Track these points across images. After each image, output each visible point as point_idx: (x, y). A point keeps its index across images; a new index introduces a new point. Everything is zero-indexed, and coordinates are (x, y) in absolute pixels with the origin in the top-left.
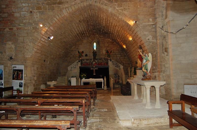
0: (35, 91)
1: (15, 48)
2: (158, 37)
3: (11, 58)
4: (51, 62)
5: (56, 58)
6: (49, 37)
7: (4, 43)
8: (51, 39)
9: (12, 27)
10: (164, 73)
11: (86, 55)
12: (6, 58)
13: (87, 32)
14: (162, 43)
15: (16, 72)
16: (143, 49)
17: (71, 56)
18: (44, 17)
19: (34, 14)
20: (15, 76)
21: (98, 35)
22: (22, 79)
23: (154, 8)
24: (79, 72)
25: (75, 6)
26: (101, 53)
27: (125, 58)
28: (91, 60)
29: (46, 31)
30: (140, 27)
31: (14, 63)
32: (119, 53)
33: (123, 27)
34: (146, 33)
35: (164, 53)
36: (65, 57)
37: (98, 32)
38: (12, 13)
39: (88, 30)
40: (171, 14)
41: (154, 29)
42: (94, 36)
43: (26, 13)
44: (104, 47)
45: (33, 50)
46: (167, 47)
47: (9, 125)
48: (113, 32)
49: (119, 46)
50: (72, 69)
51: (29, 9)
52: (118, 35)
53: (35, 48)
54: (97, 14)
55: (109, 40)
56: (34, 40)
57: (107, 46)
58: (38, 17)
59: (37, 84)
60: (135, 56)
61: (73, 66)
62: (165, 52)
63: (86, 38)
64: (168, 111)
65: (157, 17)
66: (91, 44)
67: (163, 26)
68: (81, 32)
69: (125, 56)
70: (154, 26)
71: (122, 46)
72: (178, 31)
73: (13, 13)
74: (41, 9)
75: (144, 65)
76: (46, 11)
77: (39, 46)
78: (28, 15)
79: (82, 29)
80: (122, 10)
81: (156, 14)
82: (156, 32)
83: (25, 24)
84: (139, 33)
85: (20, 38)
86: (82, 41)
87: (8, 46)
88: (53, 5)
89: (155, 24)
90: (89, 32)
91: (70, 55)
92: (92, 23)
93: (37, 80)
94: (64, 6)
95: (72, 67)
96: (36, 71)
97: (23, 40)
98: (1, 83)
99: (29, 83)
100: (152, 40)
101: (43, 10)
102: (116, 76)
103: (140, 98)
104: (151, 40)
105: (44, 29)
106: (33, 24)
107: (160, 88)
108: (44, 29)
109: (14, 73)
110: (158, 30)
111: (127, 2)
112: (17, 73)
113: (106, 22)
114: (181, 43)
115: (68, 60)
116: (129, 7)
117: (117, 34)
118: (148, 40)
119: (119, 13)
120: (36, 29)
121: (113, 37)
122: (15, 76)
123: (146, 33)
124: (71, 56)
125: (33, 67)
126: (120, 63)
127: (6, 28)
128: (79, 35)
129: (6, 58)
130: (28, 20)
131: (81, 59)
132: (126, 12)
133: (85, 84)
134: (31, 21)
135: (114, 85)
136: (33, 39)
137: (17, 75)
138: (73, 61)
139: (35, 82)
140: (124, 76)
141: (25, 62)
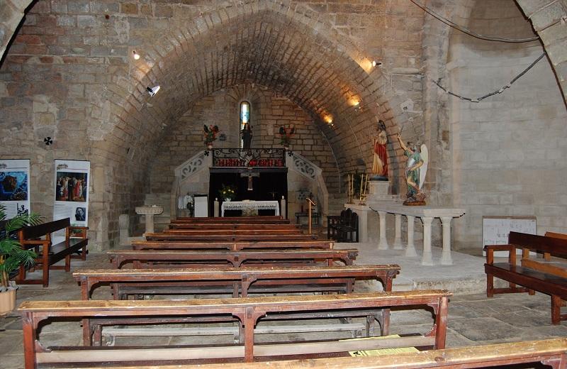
1: (60, 114)
2: (429, 104)
3: (48, 141)
6: (148, 88)
7: (25, 97)
9: (50, 54)
10: (438, 190)
11: (223, 137)
12: (31, 140)
14: (438, 119)
15: (68, 179)
16: (387, 130)
17: (180, 138)
18: (143, 34)
19: (114, 24)
20: (64, 190)
21: (255, 85)
22: (83, 199)
23: (421, 33)
25: (230, 11)
26: (263, 133)
27: (326, 149)
29: (147, 71)
30: (388, 78)
31: (58, 153)
33: (340, 72)
34: (401, 93)
35: (440, 144)
37: (259, 77)
38: (51, 16)
40: (461, 52)
41: (419, 83)
43: (91, 19)
44: (271, 117)
46: (449, 128)
47: (159, 302)
48: (303, 81)
49: (310, 117)
50: (185, 173)
51: (102, 10)
52: (317, 89)
54: (275, 34)
55: (285, 98)
58: (125, 33)
60: (359, 144)
62: (442, 142)
63: (222, 90)
64: (485, 265)
65: (428, 57)
67: (440, 79)
69: (325, 143)
70: (419, 76)
71: (319, 118)
72: (484, 98)
73: (55, 17)
74: (136, 12)
75: (410, 172)
76: (149, 19)
78: (97, 24)
80: (346, 31)
81: (426, 48)
82: (423, 91)
83: (88, 48)
84: (383, 91)
85: (75, 86)
87: (36, 107)
88: (169, 5)
89: (423, 73)
92: (252, 53)
94: (199, 10)
95: (186, 169)
97: (82, 93)
98: (23, 209)
99: (100, 210)
100: (412, 111)
101: (140, 13)
103: (393, 246)
104: (410, 110)
105: (142, 67)
106: (112, 51)
107: (452, 222)
108: (142, 67)
109: (62, 183)
110: (430, 86)
111: (360, 12)
112: (70, 182)
113: (295, 55)
114: (480, 122)
115: (171, 149)
116: (363, 25)
117: (317, 86)
118: (403, 111)
119: (338, 38)
120: (121, 65)
121: (300, 92)
122: (62, 189)
123: (401, 93)
124: (180, 138)
127: (31, 57)
129: (31, 140)
130: (96, 40)
131: (210, 147)
132: (354, 38)
133: (231, 213)
134: (105, 42)
135: (298, 217)
137: (71, 186)
140: (326, 195)
141: (90, 154)
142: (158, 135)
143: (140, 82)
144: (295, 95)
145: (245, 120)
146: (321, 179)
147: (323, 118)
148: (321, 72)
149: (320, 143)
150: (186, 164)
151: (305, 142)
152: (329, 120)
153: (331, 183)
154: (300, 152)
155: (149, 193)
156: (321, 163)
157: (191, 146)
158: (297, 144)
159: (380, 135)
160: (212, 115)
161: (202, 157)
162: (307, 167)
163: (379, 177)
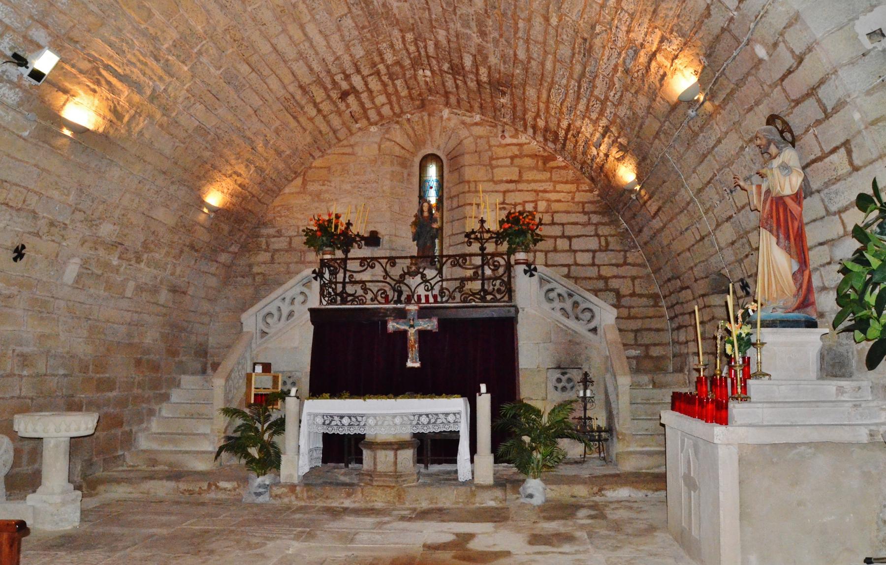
13: (374, 84)
27: (629, 260)
28: (394, 265)
32: (589, 223)
39: (381, 67)
42: (425, 114)
44: (490, 186)
55: (523, 139)
57: (511, 181)
61: (279, 309)
63: (373, 129)
79: (329, 47)
86: (348, 150)
90: (385, 78)
91: (269, 236)
95: (270, 314)
102: (564, 378)
115: (256, 269)
118: (867, 44)
126: (596, 292)
128: (319, 94)
138: (288, 264)
146: (614, 335)
149: (614, 243)
151: (577, 244)
152: (626, 174)
153: (647, 346)
156: (618, 295)
158: (555, 250)
160: (348, 187)
162: (576, 304)
163: (780, 314)
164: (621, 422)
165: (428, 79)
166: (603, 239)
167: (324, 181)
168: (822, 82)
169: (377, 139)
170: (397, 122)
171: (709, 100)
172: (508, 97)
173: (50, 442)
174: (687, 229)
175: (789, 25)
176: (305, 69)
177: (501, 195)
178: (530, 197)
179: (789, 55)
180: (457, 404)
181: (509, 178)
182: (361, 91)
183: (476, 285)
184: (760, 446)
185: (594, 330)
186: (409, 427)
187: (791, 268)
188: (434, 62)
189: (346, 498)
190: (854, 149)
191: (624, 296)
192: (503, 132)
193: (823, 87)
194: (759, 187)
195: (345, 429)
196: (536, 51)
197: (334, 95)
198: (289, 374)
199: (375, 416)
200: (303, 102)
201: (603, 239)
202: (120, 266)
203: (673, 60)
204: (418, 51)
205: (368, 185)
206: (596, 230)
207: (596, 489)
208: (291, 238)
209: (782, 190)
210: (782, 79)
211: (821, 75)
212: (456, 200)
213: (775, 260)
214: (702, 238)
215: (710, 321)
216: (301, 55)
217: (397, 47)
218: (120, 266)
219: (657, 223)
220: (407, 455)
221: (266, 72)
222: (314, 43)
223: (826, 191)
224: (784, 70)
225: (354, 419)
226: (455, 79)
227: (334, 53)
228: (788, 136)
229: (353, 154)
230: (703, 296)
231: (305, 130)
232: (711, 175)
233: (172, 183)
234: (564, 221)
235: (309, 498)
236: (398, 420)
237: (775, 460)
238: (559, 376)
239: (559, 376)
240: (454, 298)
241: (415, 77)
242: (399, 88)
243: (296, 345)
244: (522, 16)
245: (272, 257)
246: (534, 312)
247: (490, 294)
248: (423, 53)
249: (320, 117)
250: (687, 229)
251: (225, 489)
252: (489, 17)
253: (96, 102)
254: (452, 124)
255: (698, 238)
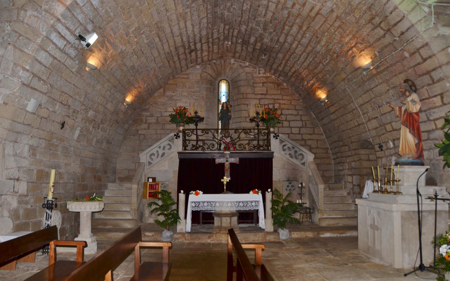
0: (184, 151)
4: (85, 133)
5: (102, 122)
8: (88, 45)
24: (177, 169)
36: (130, 122)
37: (239, 48)
42: (223, 61)
44: (253, 96)
45: (14, 74)
53: (24, 69)
56: (20, 35)
59: (26, 209)
63: (198, 67)
66: (212, 85)
68: (189, 42)
77: (41, 63)
79: (193, 31)
90: (210, 45)
91: (147, 116)
93: (27, 195)
95: (153, 154)
96: (24, 158)
102: (290, 185)
115: (140, 132)
124: (152, 120)
125: (16, 142)
136: (16, 32)
138: (156, 130)
139: (20, 202)
142: (121, 116)
143: (59, 20)
144: (280, 69)
145: (224, 99)
146: (313, 166)
147: (314, 94)
148: (320, 20)
150: (154, 149)
151: (292, 124)
152: (322, 95)
154: (287, 135)
155: (114, 181)
157: (162, 129)
158: (282, 127)
159: (409, 99)
160: (186, 94)
161: (171, 140)
162: (296, 152)
163: (411, 160)
164: (320, 205)
165: (228, 46)
166: (304, 122)
167: (174, 90)
168: (434, 70)
169: (200, 72)
170: (209, 64)
171: (375, 69)
172: (267, 56)
173: (84, 214)
174: (351, 121)
175: (423, 46)
176: (180, 40)
177: (258, 100)
178: (272, 101)
179: (420, 58)
180: (259, 197)
181: (262, 93)
182: (198, 49)
183: (255, 143)
184: (409, 212)
185: (304, 164)
186: (234, 207)
187: (415, 141)
188: (235, 38)
189: (208, 239)
190: (445, 97)
191: (313, 148)
192: (259, 71)
193: (434, 72)
194: (400, 108)
195: (205, 208)
196: (290, 39)
197: (187, 51)
198: (162, 183)
199: (219, 202)
200: (174, 55)
201: (304, 122)
202: (92, 131)
203: (361, 51)
204: (229, 33)
205: (195, 94)
206: (301, 117)
207: (316, 233)
208: (157, 117)
209: (413, 110)
210: (415, 66)
211: (434, 67)
212: (236, 102)
213: (407, 138)
214: (359, 125)
215: (358, 161)
216: (181, 35)
217: (220, 32)
218: (92, 131)
219: (333, 117)
220: (235, 219)
221: (165, 41)
222: (188, 29)
223: (428, 111)
224: (416, 63)
225: (209, 203)
226: (242, 47)
227: (194, 33)
228: (413, 88)
229: (188, 78)
230: (355, 149)
231: (170, 67)
232: (369, 99)
233: (116, 92)
234: (287, 113)
235: (192, 239)
236: (229, 205)
237: (414, 217)
238: (288, 184)
239: (288, 184)
240: (245, 148)
241: (223, 44)
242: (214, 49)
243: (167, 168)
244: (289, 24)
245: (149, 126)
246: (278, 155)
247: (262, 147)
248: (231, 34)
249: (178, 62)
250: (351, 121)
251: (149, 236)
252: (271, 23)
253: (100, 55)
254: (235, 66)
255: (356, 125)
